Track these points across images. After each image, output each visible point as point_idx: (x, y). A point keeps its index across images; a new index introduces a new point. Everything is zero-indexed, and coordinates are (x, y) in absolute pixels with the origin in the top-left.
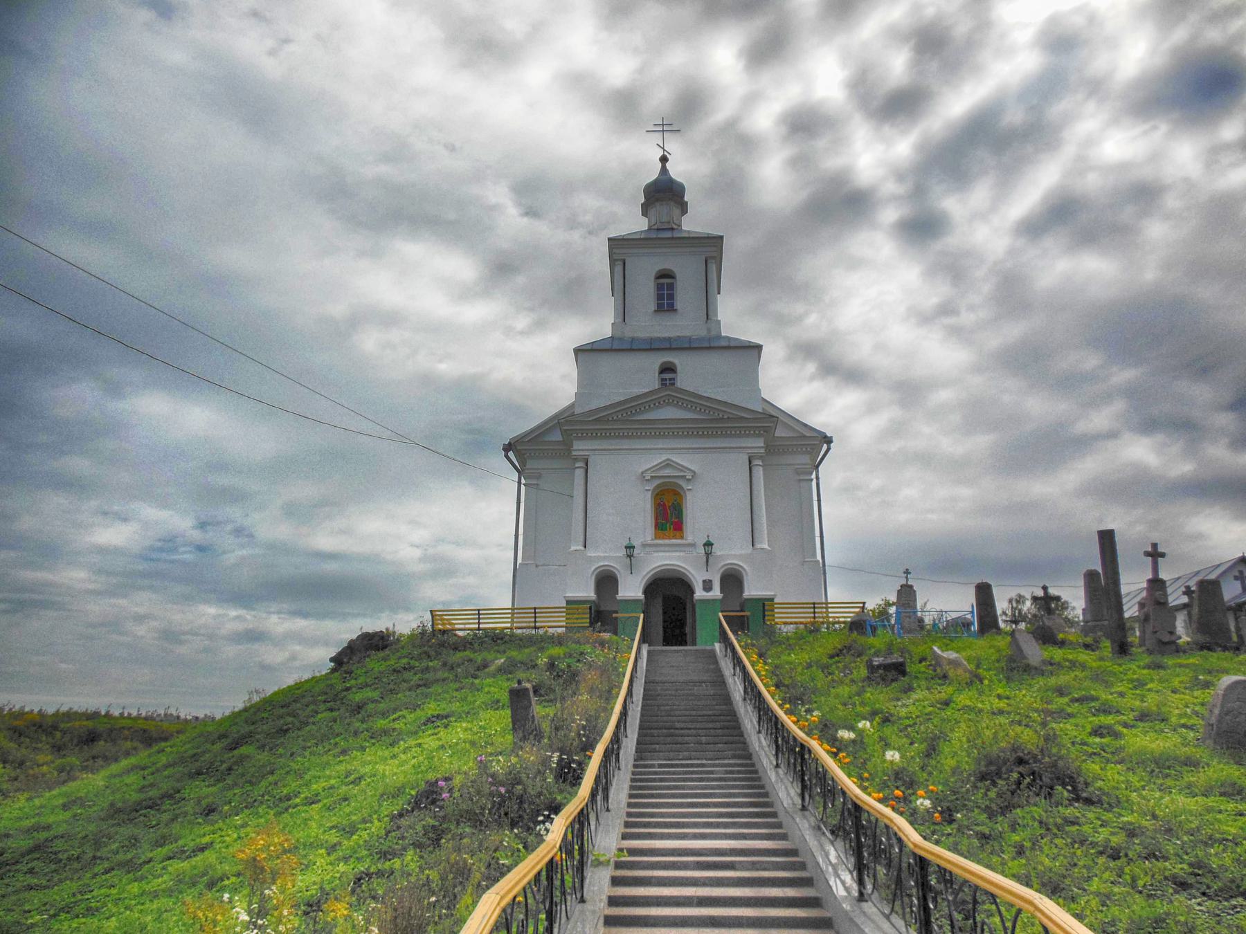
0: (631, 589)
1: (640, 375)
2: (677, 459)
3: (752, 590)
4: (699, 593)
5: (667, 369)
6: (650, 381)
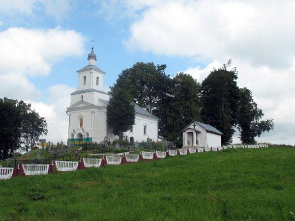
0: (75, 137)
1: (78, 98)
2: (82, 114)
3: (90, 136)
4: (83, 137)
5: (82, 96)
6: (80, 99)
